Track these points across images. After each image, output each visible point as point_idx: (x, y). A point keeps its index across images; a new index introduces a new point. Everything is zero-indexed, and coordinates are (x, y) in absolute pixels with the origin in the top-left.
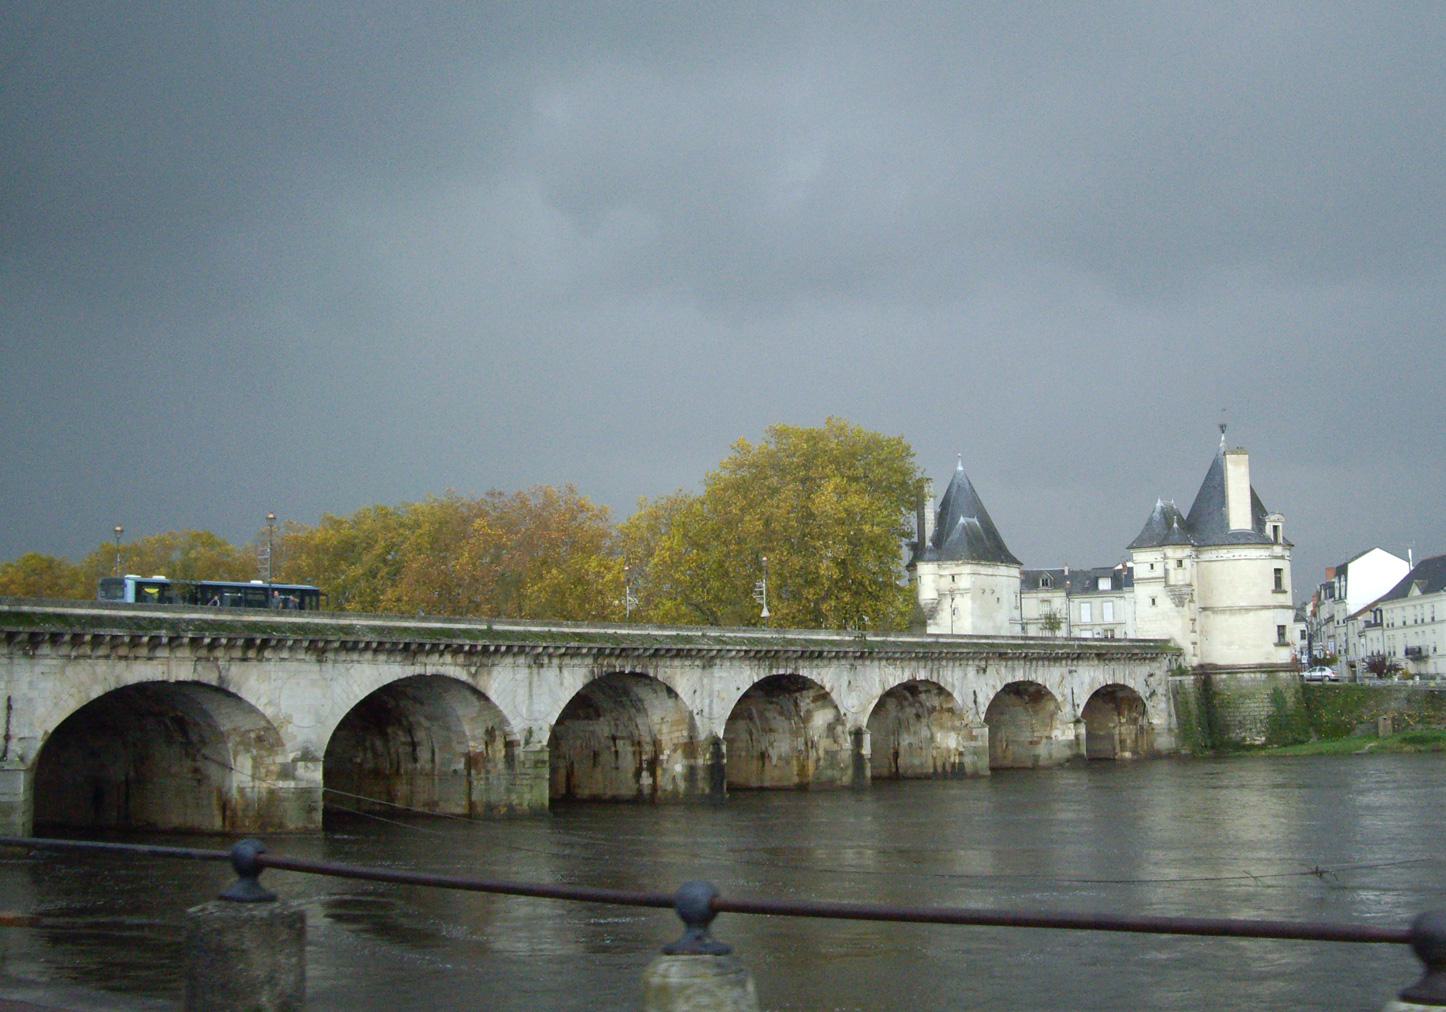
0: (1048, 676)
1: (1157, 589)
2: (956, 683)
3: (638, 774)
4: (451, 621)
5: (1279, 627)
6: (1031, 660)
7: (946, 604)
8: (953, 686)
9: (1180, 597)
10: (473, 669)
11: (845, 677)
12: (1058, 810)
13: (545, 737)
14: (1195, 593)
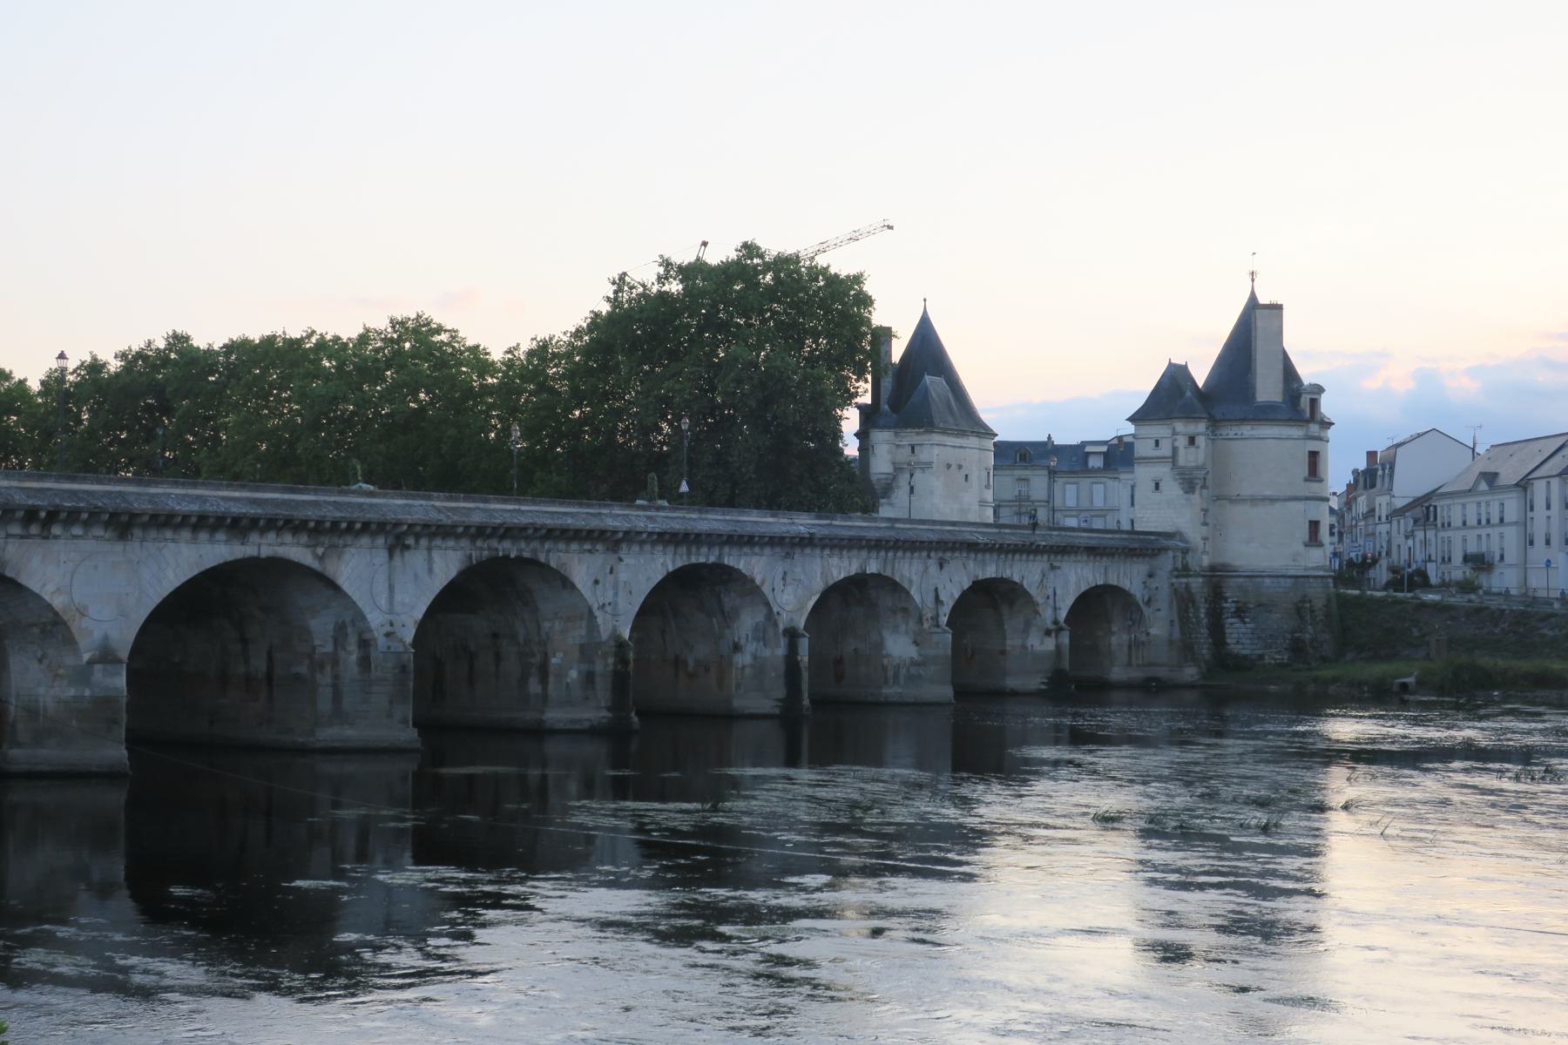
0: (1027, 573)
1: (1163, 471)
2: (914, 578)
3: (523, 681)
4: (292, 491)
6: (1007, 553)
7: (903, 480)
8: (911, 581)
9: (1189, 483)
10: (320, 551)
13: (409, 635)
14: (1210, 477)
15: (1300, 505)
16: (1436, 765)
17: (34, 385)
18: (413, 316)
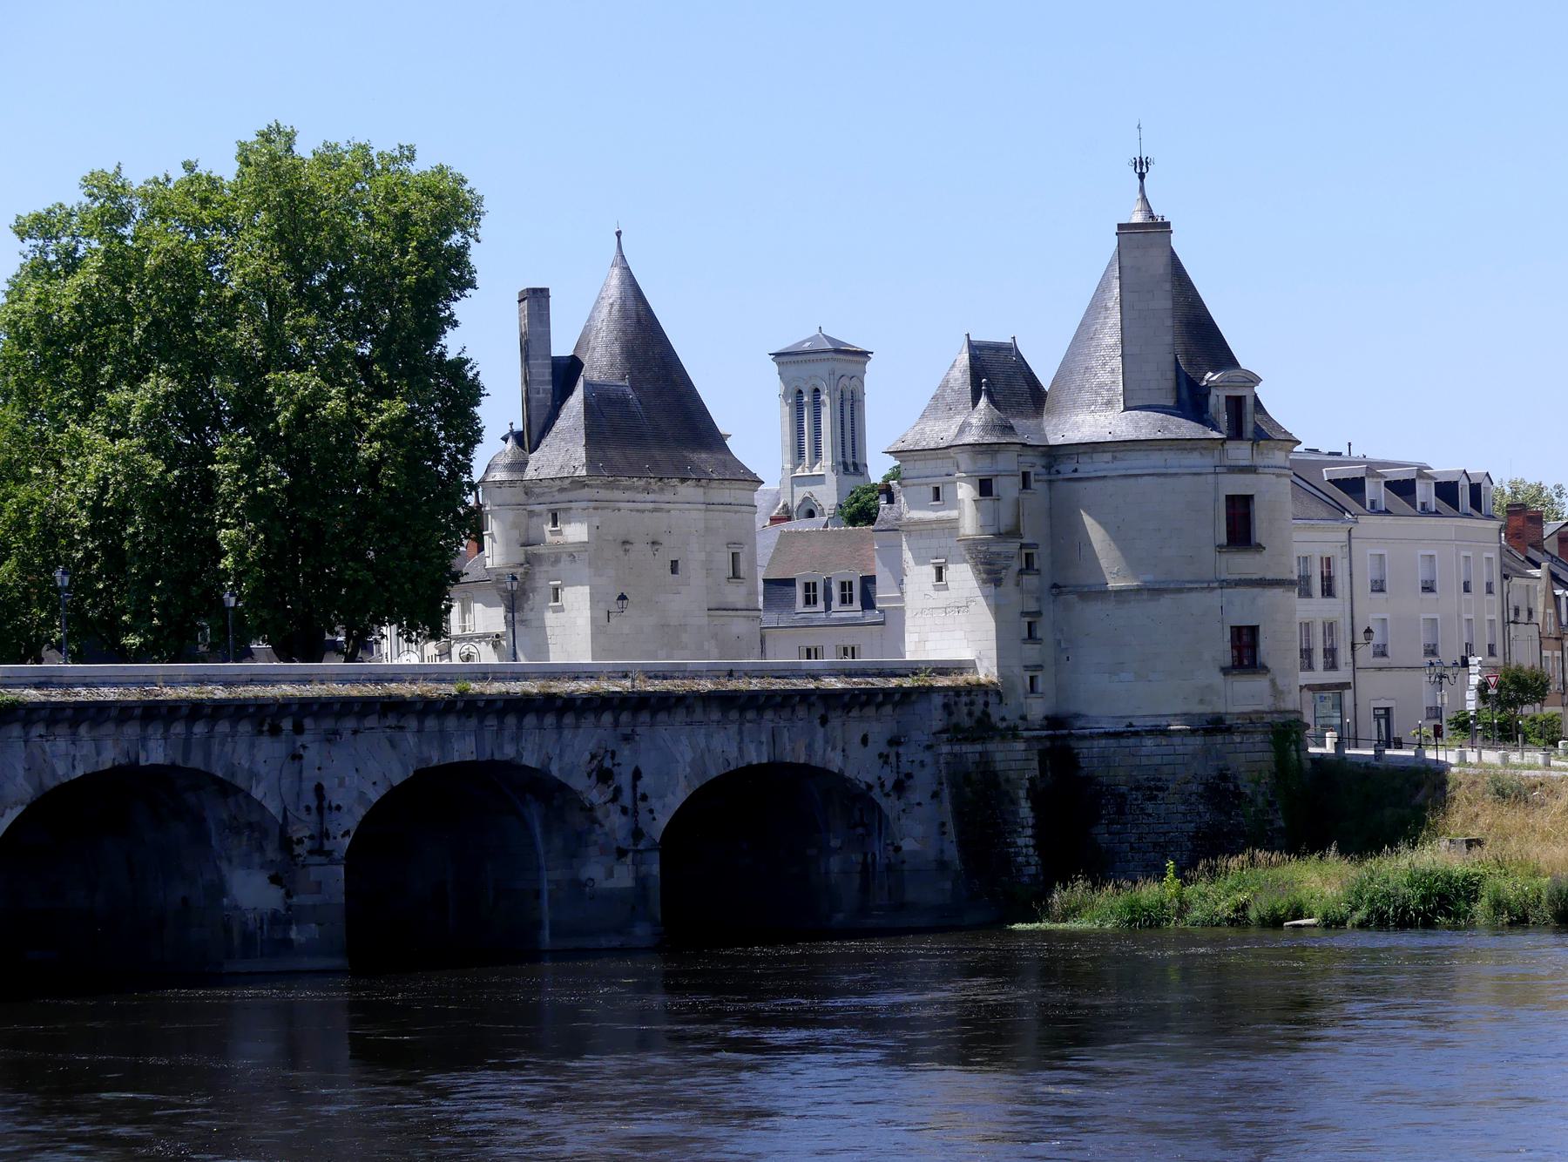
2: (263, 769)
5: (1237, 632)
8: (253, 775)
15: (1215, 599)
16: (1127, 1064)
17: (227, 169)
18: (179, 174)
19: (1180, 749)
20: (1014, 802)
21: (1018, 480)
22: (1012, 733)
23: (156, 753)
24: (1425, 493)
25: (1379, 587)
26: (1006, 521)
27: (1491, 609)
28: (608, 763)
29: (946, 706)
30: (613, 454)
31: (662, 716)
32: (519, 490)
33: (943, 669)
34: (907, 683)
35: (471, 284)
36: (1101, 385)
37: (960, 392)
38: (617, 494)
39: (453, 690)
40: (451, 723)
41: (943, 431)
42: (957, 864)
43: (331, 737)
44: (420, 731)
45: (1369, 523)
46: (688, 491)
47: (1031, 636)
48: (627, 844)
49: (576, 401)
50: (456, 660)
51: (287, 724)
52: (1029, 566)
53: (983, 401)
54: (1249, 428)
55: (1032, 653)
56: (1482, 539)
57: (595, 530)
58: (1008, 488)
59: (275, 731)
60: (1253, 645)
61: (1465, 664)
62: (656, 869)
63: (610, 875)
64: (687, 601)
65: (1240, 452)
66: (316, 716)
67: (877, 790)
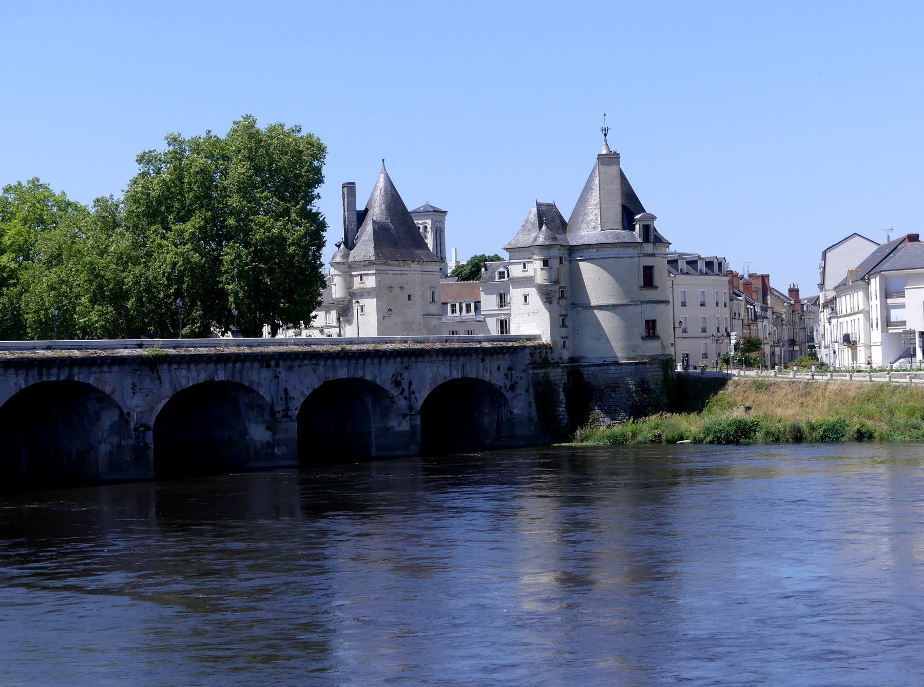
5: (647, 322)
8: (259, 384)
11: (129, 381)
12: (691, 473)
15: (638, 309)
18: (204, 135)
19: (625, 371)
20: (558, 393)
21: (558, 260)
22: (556, 365)
23: (221, 376)
24: (701, 266)
25: (684, 304)
26: (554, 277)
27: (725, 313)
28: (399, 379)
29: (531, 354)
30: (385, 251)
31: (420, 359)
32: (346, 266)
33: (529, 338)
34: (516, 344)
35: (322, 182)
36: (591, 220)
37: (533, 223)
38: (387, 268)
39: (339, 348)
40: (337, 362)
41: (526, 240)
42: (536, 419)
43: (290, 369)
44: (325, 366)
45: (681, 277)
46: (415, 266)
47: (564, 325)
48: (407, 412)
49: (368, 228)
50: (304, 337)
51: (273, 363)
52: (562, 296)
53: (544, 227)
54: (652, 238)
55: (564, 331)
56: (717, 286)
57: (378, 282)
58: (555, 263)
59: (268, 366)
60: (654, 328)
61: (729, 335)
62: (419, 422)
63: (400, 425)
64: (414, 312)
65: (649, 248)
66: (285, 360)
67: (503, 389)
